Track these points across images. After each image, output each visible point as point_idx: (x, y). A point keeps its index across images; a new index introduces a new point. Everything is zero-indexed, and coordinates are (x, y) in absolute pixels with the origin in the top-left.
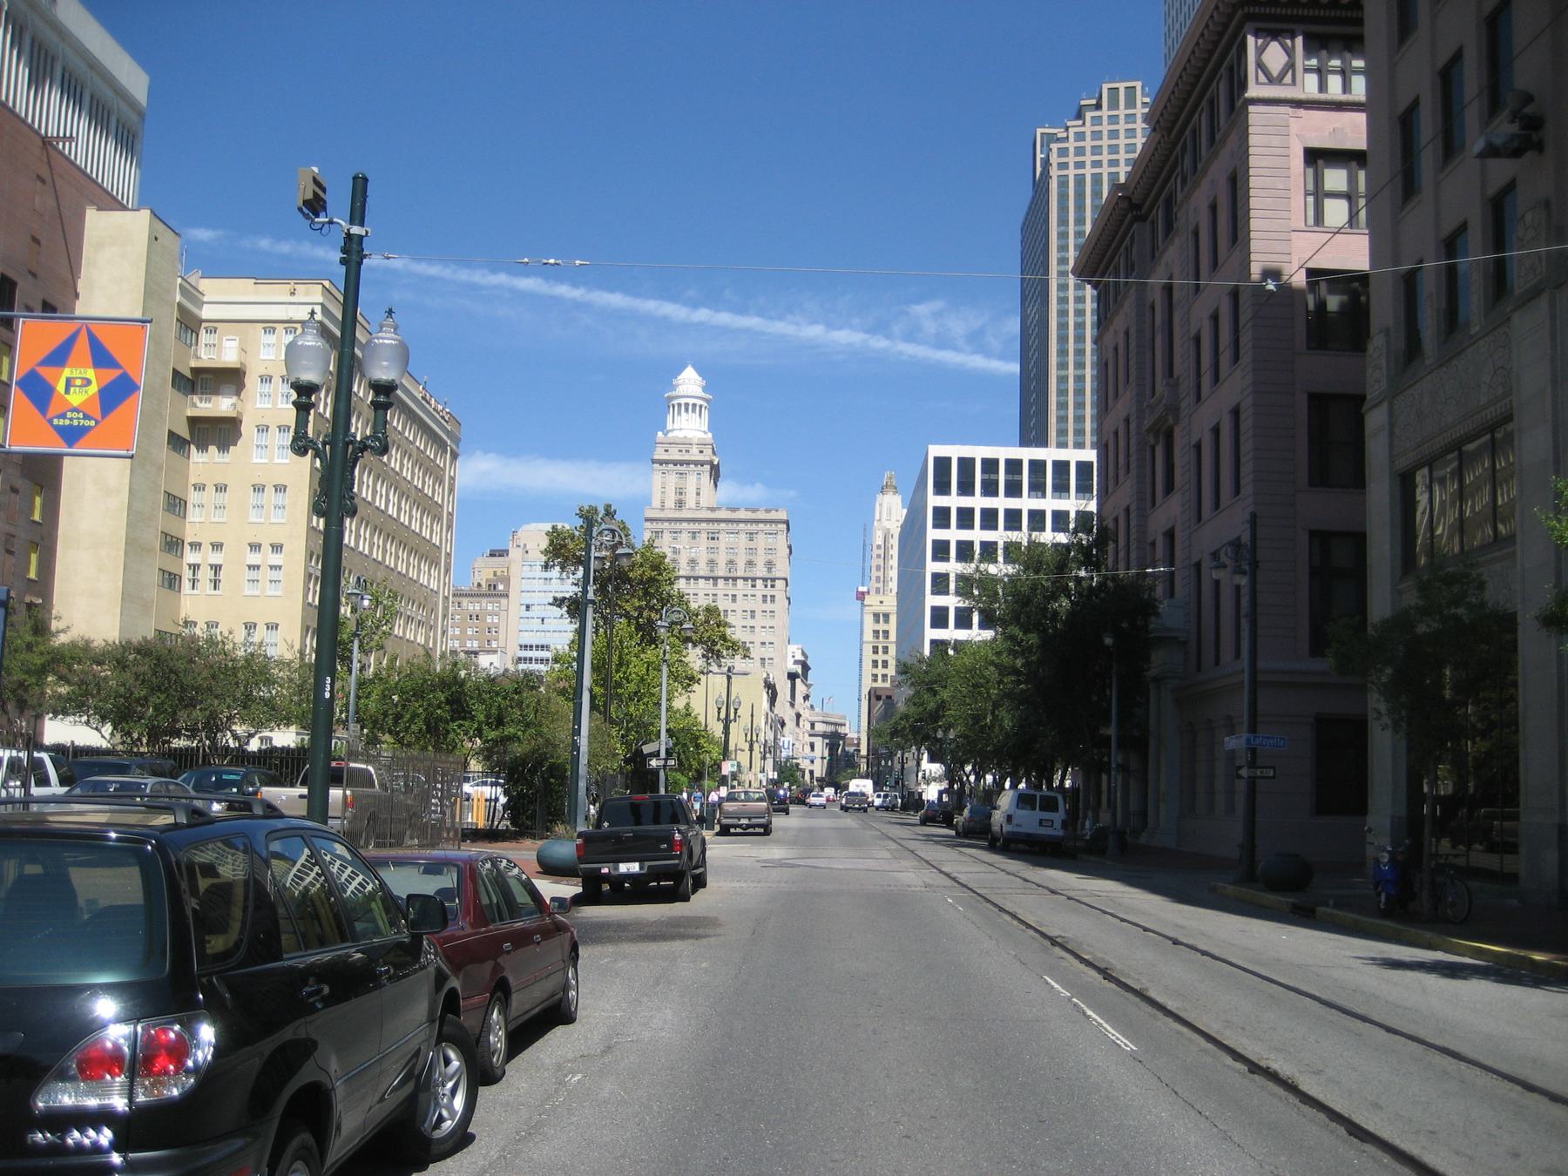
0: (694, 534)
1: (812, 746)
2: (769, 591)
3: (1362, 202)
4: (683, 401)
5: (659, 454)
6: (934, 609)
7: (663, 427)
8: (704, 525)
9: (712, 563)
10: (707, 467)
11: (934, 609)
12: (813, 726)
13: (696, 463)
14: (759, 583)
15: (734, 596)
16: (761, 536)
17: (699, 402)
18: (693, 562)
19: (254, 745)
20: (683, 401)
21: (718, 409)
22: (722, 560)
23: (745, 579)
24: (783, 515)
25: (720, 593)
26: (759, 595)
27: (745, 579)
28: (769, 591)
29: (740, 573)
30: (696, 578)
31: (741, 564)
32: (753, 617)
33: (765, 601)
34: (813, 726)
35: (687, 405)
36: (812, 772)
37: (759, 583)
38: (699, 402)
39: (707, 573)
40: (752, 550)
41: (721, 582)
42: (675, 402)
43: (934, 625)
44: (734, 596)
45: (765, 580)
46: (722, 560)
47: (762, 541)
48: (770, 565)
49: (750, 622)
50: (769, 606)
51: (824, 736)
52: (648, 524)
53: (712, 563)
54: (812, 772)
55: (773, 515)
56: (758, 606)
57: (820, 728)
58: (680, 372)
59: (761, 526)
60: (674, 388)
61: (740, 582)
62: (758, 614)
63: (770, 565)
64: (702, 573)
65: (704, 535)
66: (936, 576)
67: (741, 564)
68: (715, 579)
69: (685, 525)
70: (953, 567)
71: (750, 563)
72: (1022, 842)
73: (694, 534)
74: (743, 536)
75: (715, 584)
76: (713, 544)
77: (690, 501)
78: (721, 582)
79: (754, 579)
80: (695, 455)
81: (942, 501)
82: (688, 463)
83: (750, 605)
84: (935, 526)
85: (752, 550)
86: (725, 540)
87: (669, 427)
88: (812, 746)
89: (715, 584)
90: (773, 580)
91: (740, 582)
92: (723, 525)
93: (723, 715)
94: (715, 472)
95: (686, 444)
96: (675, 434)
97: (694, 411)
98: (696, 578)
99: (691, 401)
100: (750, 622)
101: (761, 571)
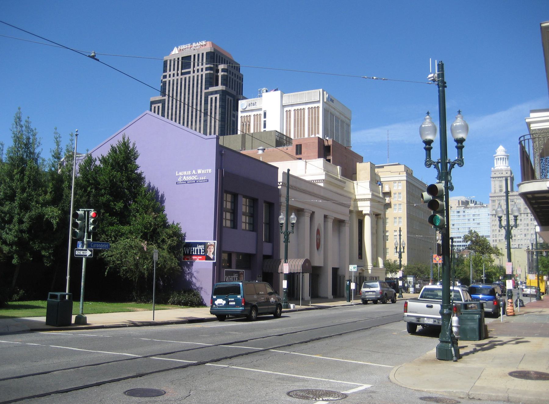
5: (493, 175)
26: (530, 218)
42: (497, 157)
52: (491, 198)
61: (523, 215)
62: (529, 225)
87: (495, 165)
91: (523, 215)
93: (504, 223)
100: (527, 227)
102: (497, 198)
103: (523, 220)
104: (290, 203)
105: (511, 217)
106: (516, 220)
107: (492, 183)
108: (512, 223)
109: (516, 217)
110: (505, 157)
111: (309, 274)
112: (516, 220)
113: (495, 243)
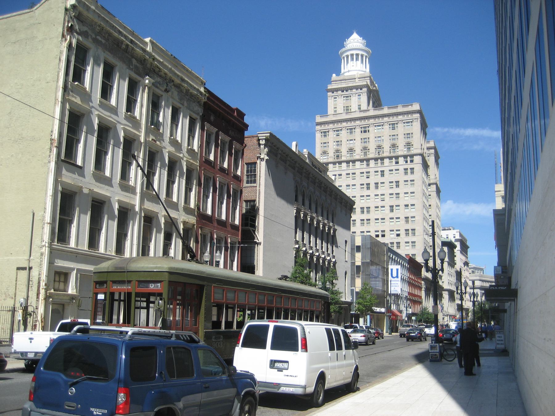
2: (409, 166)
3: (496, 288)
4: (349, 53)
8: (358, 122)
9: (365, 149)
10: (365, 90)
12: (473, 283)
13: (357, 88)
14: (401, 160)
15: (382, 172)
16: (400, 125)
17: (360, 53)
20: (349, 53)
22: (372, 146)
25: (372, 171)
26: (401, 168)
27: (390, 158)
28: (409, 166)
29: (386, 154)
30: (354, 161)
32: (397, 186)
33: (406, 173)
34: (473, 283)
35: (352, 55)
37: (401, 160)
38: (360, 53)
39: (362, 157)
42: (344, 55)
44: (382, 172)
45: (405, 157)
46: (372, 146)
48: (409, 145)
50: (409, 177)
51: (481, 288)
52: (318, 128)
53: (365, 149)
56: (401, 177)
57: (478, 283)
59: (400, 117)
60: (343, 46)
62: (401, 183)
63: (409, 145)
64: (357, 157)
65: (358, 130)
68: (368, 160)
71: (394, 146)
72: (78, 75)
74: (387, 127)
75: (368, 165)
78: (372, 163)
79: (397, 157)
80: (358, 83)
82: (351, 88)
83: (394, 178)
86: (373, 131)
89: (368, 165)
90: (412, 156)
91: (386, 161)
92: (372, 121)
97: (357, 59)
98: (354, 161)
99: (354, 52)
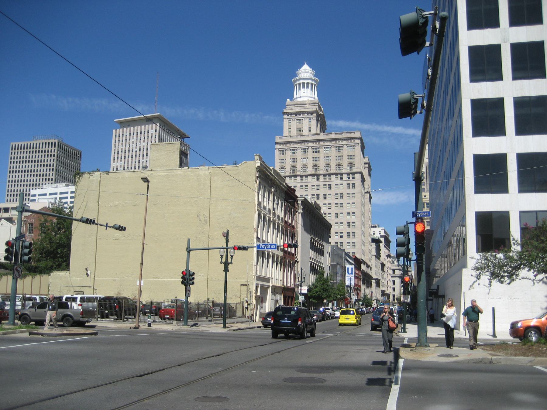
0: (305, 150)
1: (394, 282)
2: (351, 181)
4: (301, 82)
5: (288, 110)
6: (474, 51)
7: (291, 98)
8: (310, 144)
11: (476, 104)
13: (308, 113)
14: (345, 176)
15: (330, 185)
16: (345, 148)
17: (310, 82)
18: (304, 167)
19: (519, 248)
20: (301, 82)
21: (322, 86)
23: (336, 174)
24: (358, 134)
25: (321, 184)
26: (345, 183)
27: (336, 174)
28: (351, 181)
29: (333, 171)
30: (307, 176)
31: (333, 165)
32: (342, 197)
33: (349, 187)
35: (304, 83)
36: (394, 296)
37: (345, 176)
38: (310, 82)
39: (313, 173)
40: (339, 157)
41: (321, 178)
42: (297, 83)
43: (482, 187)
44: (330, 185)
45: (348, 174)
47: (345, 151)
48: (351, 165)
49: (340, 201)
50: (351, 190)
52: (277, 146)
54: (394, 296)
55: (352, 135)
56: (344, 190)
58: (300, 67)
59: (345, 142)
61: (333, 177)
62: (345, 196)
63: (351, 165)
64: (310, 173)
65: (310, 150)
66: (480, 161)
67: (333, 165)
68: (318, 175)
69: (299, 145)
70: (509, 89)
71: (339, 165)
73: (305, 150)
74: (334, 149)
76: (316, 155)
77: (306, 131)
78: (321, 178)
79: (342, 174)
80: (309, 108)
81: (484, 37)
82: (303, 113)
84: (472, 25)
85: (339, 157)
87: (295, 96)
88: (394, 282)
89: (318, 179)
90: (354, 174)
91: (333, 177)
92: (322, 143)
93: (224, 260)
94: (322, 121)
95: (304, 104)
96: (299, 100)
97: (308, 87)
98: (307, 176)
99: (306, 81)
100: (340, 201)
101: (345, 169)
102: (288, 145)
103: (333, 186)
104: (74, 221)
105: (229, 257)
106: (232, 259)
107: (286, 124)
108: (229, 260)
109: (232, 256)
110: (314, 83)
111: (428, 327)
112: (232, 259)
113: (304, 193)
